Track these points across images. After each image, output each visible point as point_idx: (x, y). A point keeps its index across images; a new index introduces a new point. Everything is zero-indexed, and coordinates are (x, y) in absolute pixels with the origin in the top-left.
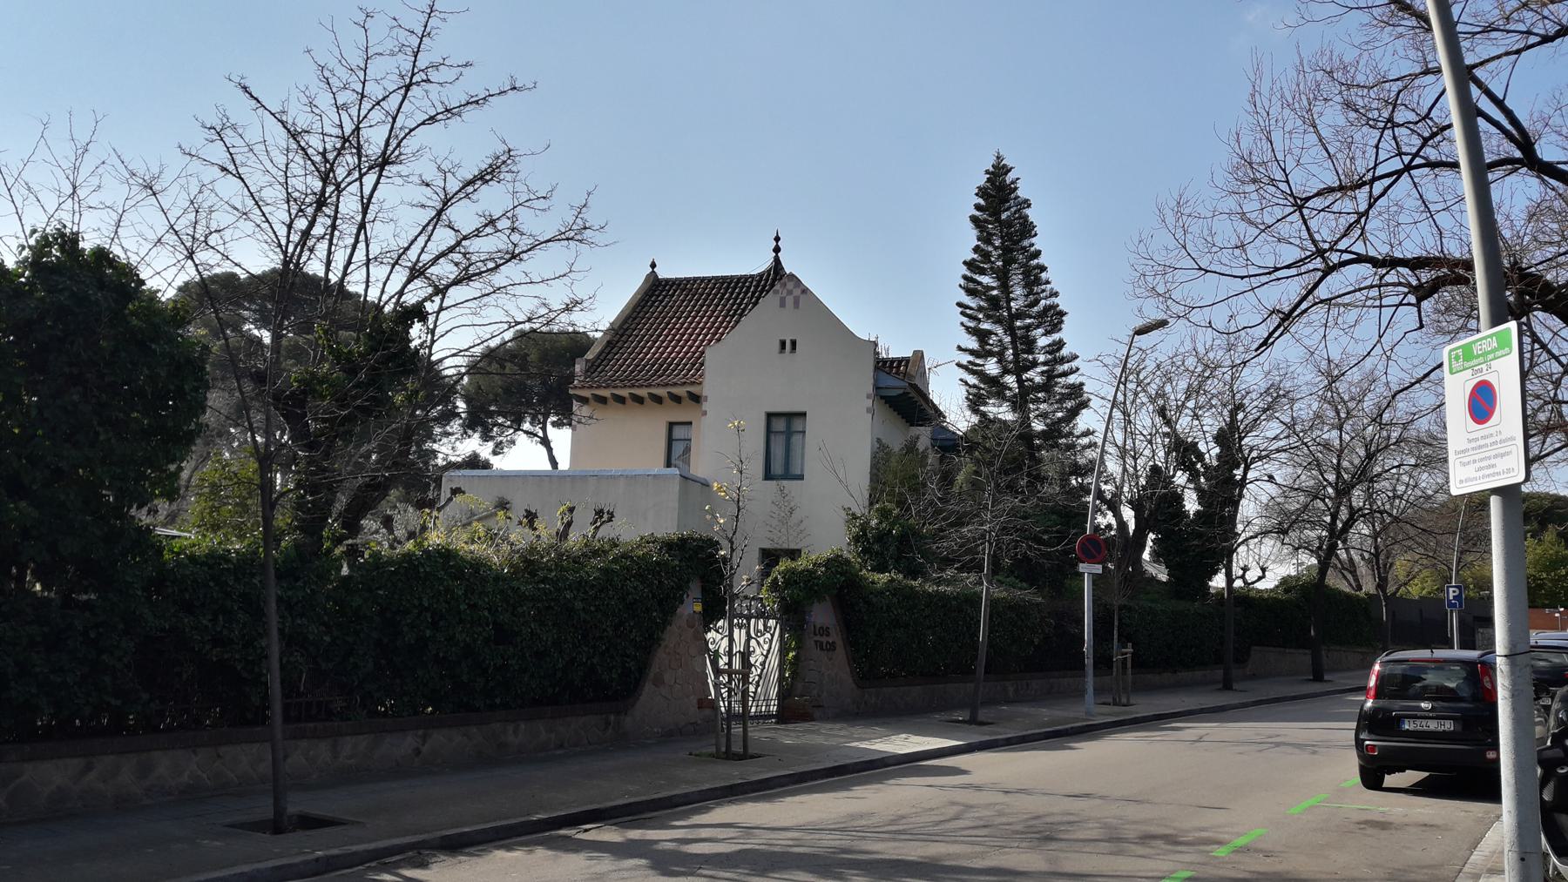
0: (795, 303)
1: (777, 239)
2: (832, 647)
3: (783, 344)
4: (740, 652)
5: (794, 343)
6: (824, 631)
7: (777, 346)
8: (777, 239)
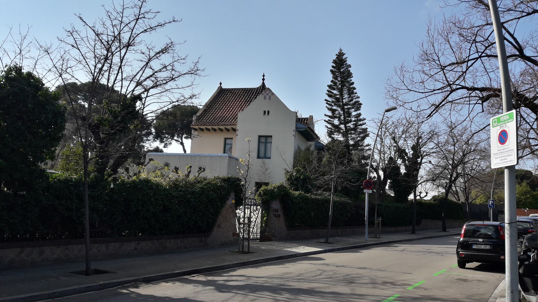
0: (270, 98)
1: (264, 76)
2: (279, 216)
3: (265, 112)
4: (247, 217)
5: (268, 112)
6: (277, 211)
7: (263, 112)
8: (264, 76)
